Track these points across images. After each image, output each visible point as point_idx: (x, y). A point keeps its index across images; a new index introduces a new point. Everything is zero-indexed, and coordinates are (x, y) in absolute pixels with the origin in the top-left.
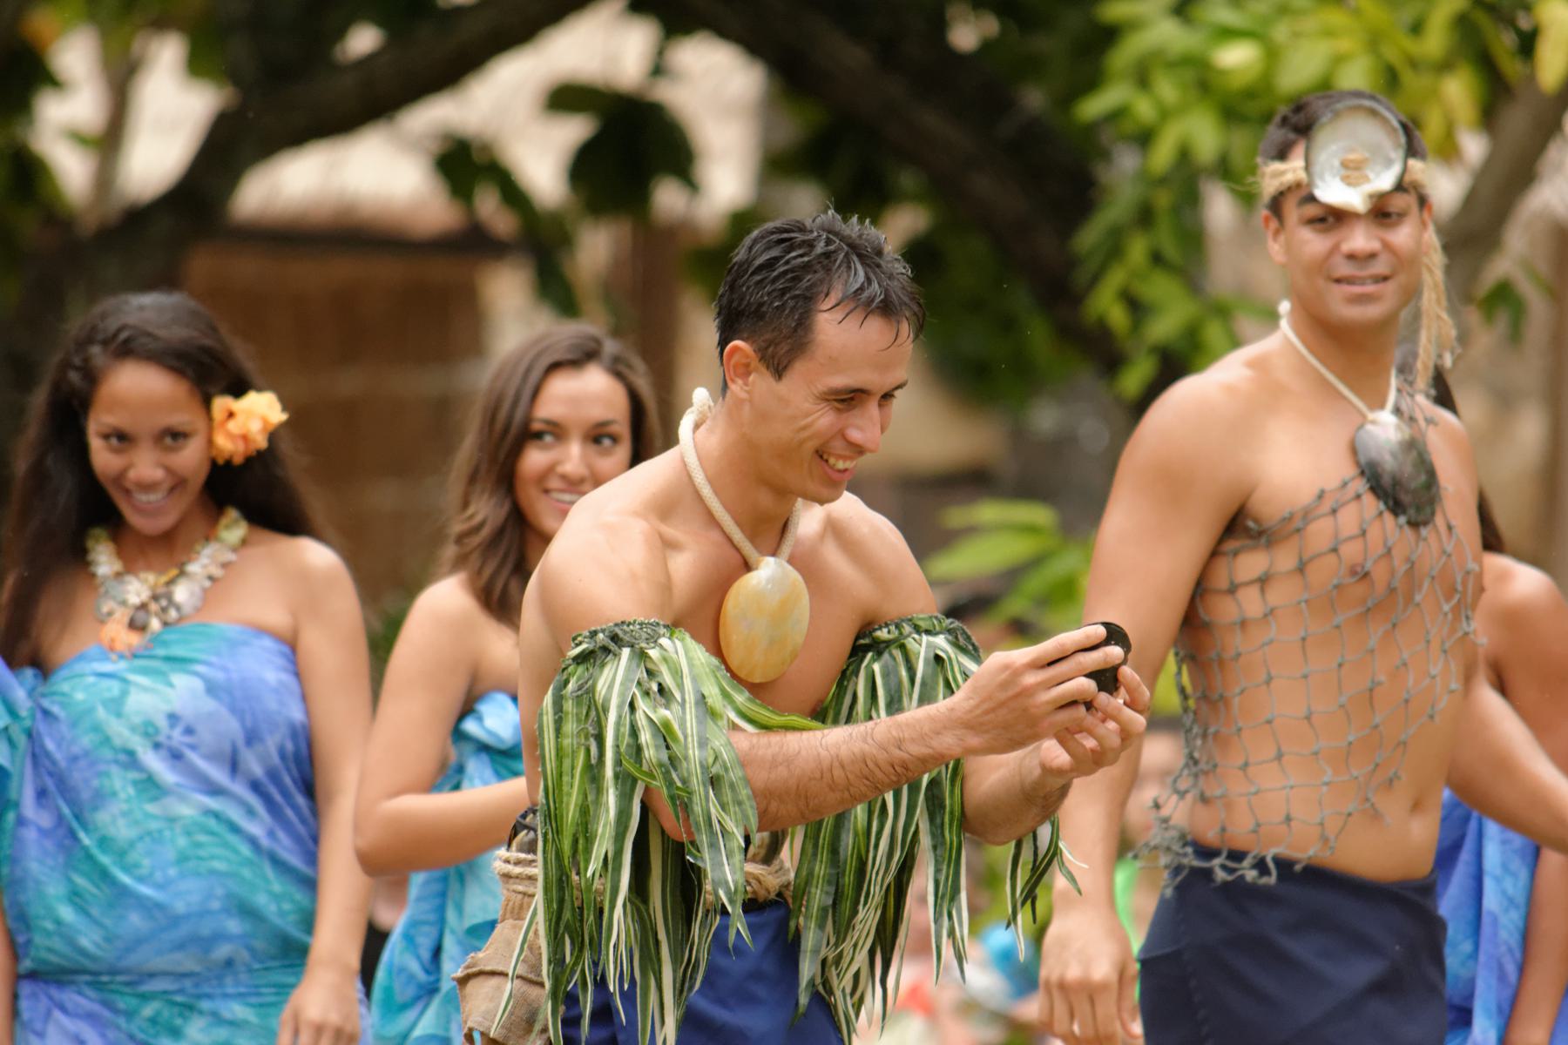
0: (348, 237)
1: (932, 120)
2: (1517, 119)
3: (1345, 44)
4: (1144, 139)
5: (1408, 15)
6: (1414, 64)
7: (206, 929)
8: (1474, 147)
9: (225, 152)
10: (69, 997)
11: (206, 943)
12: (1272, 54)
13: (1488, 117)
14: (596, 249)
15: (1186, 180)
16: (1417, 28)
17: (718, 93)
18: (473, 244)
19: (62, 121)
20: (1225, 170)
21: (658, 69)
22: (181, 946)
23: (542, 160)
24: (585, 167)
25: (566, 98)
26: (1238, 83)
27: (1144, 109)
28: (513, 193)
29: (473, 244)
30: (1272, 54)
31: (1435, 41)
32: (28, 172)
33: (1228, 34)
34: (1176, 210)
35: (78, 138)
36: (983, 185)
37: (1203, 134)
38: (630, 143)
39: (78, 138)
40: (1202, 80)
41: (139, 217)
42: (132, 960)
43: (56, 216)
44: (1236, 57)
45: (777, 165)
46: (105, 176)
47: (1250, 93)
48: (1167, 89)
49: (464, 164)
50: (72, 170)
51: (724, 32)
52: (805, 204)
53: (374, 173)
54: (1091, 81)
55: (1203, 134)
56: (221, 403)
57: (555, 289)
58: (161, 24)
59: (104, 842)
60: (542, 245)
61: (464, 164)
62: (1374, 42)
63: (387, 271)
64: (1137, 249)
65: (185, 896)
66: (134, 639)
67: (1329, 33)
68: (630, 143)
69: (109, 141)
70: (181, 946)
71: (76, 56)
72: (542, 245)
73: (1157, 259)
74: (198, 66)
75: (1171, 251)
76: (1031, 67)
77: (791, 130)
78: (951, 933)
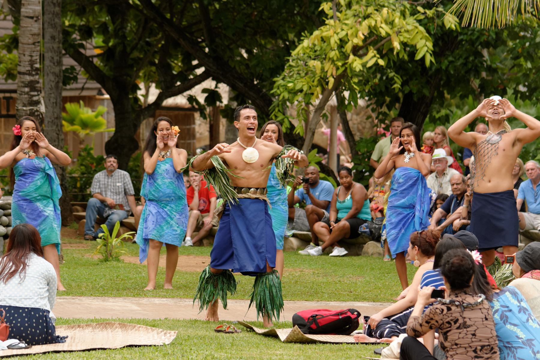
0: (177, 108)
1: (251, 93)
2: (326, 93)
3: (304, 83)
4: (279, 95)
5: (312, 80)
6: (313, 86)
7: (170, 195)
8: (321, 96)
9: (161, 98)
10: (153, 203)
11: (170, 197)
12: (295, 85)
13: (322, 93)
14: (208, 110)
15: (284, 101)
16: (313, 82)
17: (224, 89)
18: (193, 109)
19: (140, 93)
20: (288, 100)
21: (216, 87)
22: (167, 197)
23: (201, 99)
24: (206, 100)
25: (204, 91)
26: (290, 88)
27: (279, 92)
28: (198, 103)
29: (193, 109)
30: (295, 85)
31: (316, 83)
32: (137, 100)
33: (289, 82)
34: (282, 104)
35: (142, 95)
36: (258, 101)
37: (286, 95)
38: (213, 96)
39: (142, 95)
40: (286, 88)
41: (150, 106)
42: (161, 199)
43: (140, 106)
44: (290, 85)
45: (231, 99)
46: (145, 101)
47: (292, 90)
48: (281, 89)
49: (191, 99)
50: (142, 99)
51: (225, 83)
52: (235, 104)
53: (180, 100)
54: (272, 89)
55: (286, 95)
56: (173, 127)
57: (203, 115)
58: (152, 82)
59: (158, 184)
60: (201, 110)
61: (191, 99)
62: (308, 83)
63: (182, 113)
64: (277, 110)
65: (168, 191)
66: (163, 159)
67: (302, 82)
68: (213, 96)
69: (146, 96)
70: (167, 197)
71: (142, 85)
72: (201, 110)
73: (279, 111)
74: (157, 87)
75: (281, 110)
76: (264, 86)
77: (233, 95)
78: (406, 222)
